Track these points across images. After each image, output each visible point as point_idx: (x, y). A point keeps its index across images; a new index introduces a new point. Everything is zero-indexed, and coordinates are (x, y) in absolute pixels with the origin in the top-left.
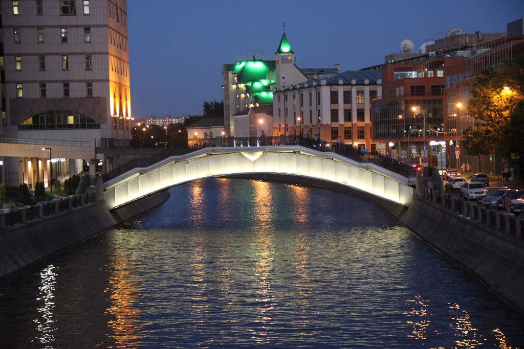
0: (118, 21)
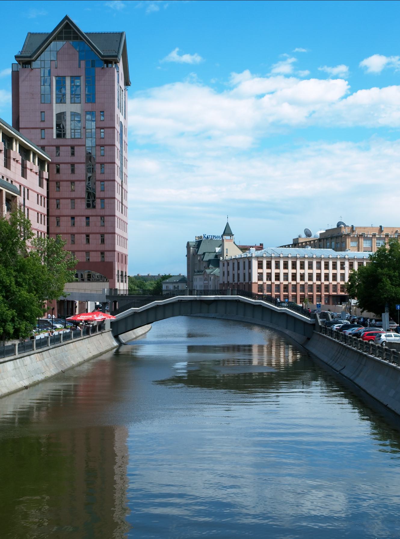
0: (122, 213)
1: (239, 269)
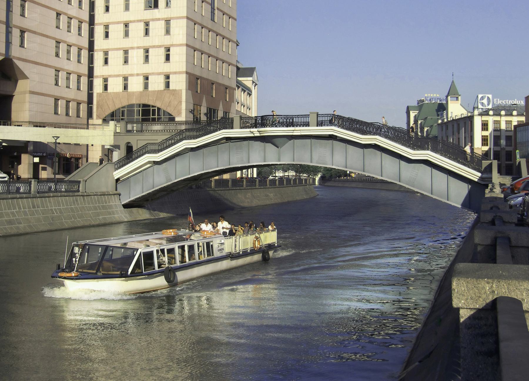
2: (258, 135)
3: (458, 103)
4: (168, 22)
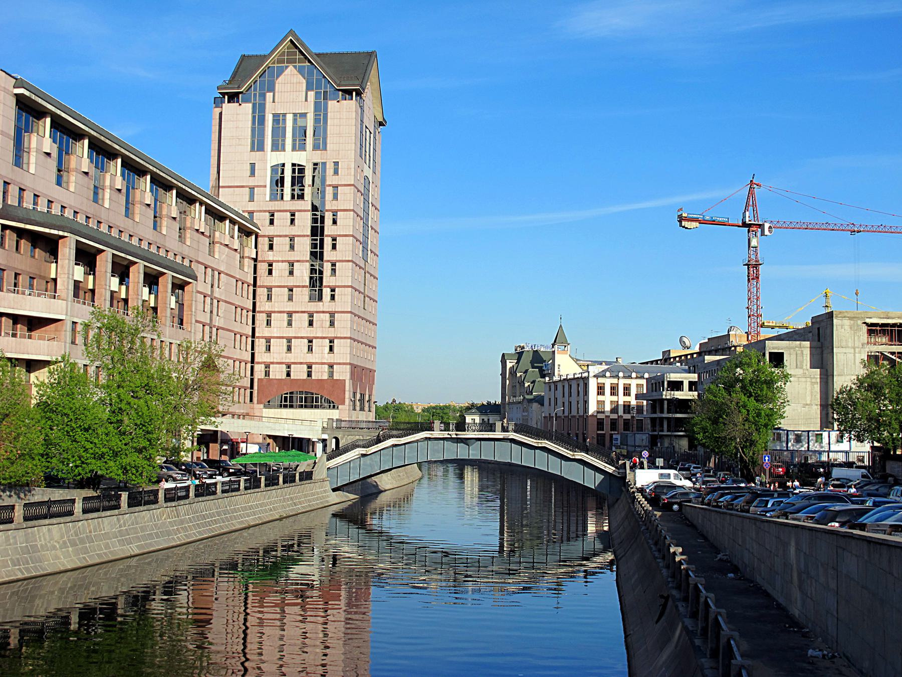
1: (570, 395)
2: (455, 436)
3: (567, 354)
4: (332, 314)
